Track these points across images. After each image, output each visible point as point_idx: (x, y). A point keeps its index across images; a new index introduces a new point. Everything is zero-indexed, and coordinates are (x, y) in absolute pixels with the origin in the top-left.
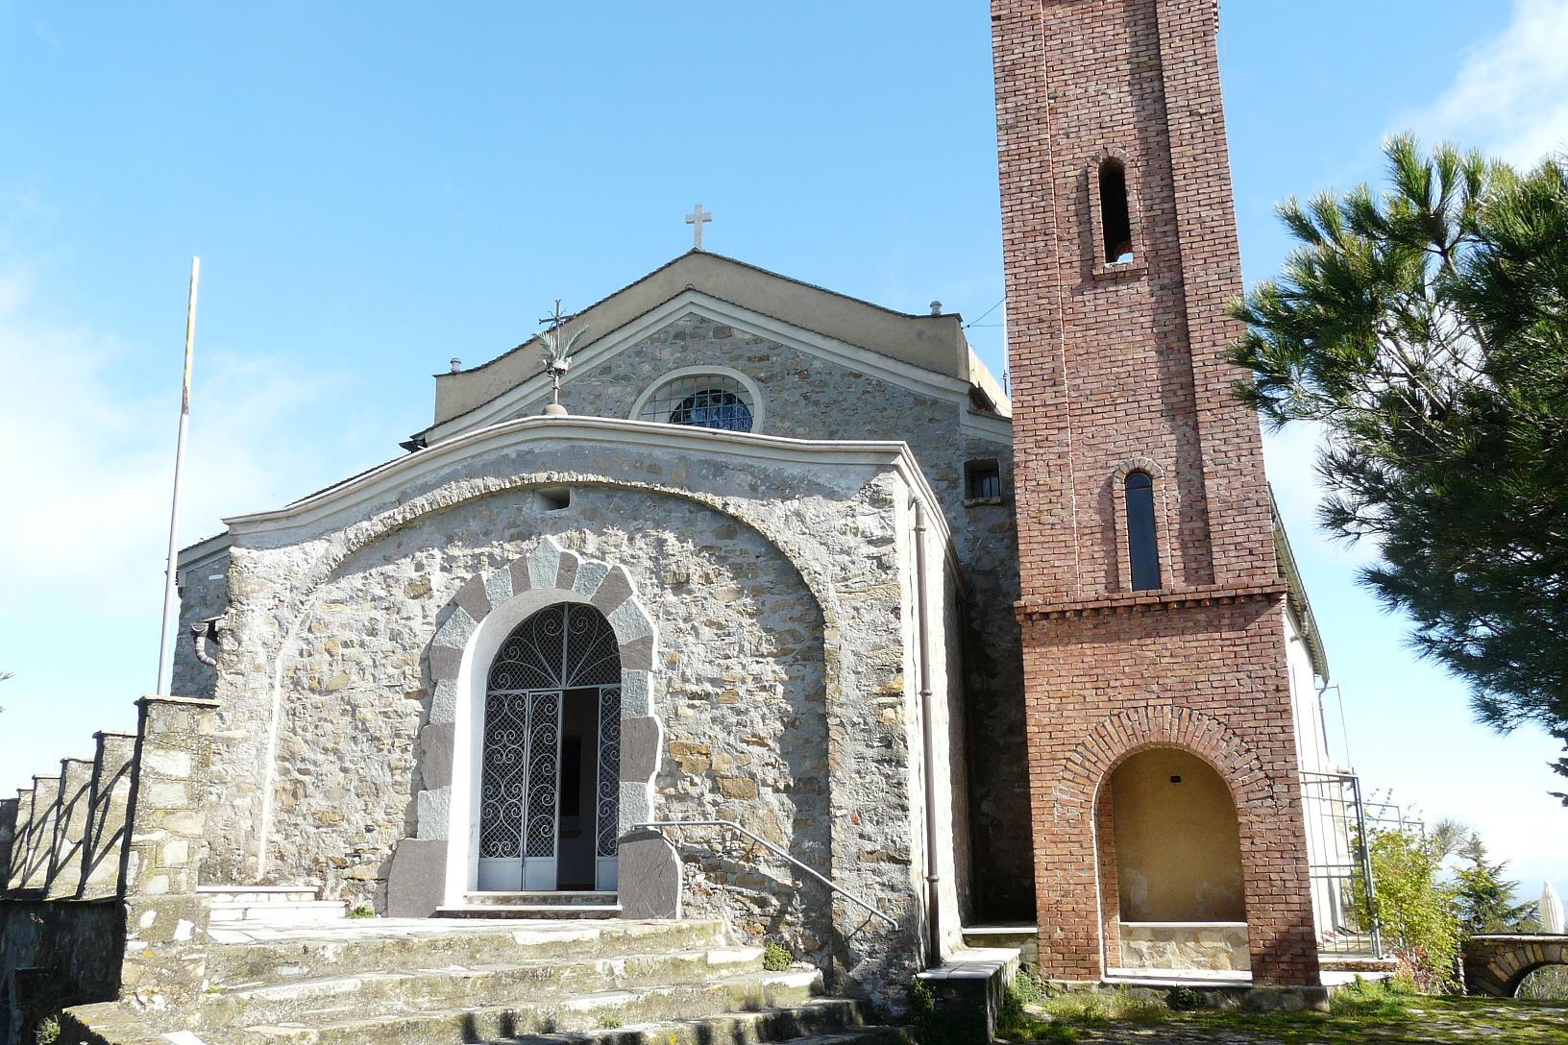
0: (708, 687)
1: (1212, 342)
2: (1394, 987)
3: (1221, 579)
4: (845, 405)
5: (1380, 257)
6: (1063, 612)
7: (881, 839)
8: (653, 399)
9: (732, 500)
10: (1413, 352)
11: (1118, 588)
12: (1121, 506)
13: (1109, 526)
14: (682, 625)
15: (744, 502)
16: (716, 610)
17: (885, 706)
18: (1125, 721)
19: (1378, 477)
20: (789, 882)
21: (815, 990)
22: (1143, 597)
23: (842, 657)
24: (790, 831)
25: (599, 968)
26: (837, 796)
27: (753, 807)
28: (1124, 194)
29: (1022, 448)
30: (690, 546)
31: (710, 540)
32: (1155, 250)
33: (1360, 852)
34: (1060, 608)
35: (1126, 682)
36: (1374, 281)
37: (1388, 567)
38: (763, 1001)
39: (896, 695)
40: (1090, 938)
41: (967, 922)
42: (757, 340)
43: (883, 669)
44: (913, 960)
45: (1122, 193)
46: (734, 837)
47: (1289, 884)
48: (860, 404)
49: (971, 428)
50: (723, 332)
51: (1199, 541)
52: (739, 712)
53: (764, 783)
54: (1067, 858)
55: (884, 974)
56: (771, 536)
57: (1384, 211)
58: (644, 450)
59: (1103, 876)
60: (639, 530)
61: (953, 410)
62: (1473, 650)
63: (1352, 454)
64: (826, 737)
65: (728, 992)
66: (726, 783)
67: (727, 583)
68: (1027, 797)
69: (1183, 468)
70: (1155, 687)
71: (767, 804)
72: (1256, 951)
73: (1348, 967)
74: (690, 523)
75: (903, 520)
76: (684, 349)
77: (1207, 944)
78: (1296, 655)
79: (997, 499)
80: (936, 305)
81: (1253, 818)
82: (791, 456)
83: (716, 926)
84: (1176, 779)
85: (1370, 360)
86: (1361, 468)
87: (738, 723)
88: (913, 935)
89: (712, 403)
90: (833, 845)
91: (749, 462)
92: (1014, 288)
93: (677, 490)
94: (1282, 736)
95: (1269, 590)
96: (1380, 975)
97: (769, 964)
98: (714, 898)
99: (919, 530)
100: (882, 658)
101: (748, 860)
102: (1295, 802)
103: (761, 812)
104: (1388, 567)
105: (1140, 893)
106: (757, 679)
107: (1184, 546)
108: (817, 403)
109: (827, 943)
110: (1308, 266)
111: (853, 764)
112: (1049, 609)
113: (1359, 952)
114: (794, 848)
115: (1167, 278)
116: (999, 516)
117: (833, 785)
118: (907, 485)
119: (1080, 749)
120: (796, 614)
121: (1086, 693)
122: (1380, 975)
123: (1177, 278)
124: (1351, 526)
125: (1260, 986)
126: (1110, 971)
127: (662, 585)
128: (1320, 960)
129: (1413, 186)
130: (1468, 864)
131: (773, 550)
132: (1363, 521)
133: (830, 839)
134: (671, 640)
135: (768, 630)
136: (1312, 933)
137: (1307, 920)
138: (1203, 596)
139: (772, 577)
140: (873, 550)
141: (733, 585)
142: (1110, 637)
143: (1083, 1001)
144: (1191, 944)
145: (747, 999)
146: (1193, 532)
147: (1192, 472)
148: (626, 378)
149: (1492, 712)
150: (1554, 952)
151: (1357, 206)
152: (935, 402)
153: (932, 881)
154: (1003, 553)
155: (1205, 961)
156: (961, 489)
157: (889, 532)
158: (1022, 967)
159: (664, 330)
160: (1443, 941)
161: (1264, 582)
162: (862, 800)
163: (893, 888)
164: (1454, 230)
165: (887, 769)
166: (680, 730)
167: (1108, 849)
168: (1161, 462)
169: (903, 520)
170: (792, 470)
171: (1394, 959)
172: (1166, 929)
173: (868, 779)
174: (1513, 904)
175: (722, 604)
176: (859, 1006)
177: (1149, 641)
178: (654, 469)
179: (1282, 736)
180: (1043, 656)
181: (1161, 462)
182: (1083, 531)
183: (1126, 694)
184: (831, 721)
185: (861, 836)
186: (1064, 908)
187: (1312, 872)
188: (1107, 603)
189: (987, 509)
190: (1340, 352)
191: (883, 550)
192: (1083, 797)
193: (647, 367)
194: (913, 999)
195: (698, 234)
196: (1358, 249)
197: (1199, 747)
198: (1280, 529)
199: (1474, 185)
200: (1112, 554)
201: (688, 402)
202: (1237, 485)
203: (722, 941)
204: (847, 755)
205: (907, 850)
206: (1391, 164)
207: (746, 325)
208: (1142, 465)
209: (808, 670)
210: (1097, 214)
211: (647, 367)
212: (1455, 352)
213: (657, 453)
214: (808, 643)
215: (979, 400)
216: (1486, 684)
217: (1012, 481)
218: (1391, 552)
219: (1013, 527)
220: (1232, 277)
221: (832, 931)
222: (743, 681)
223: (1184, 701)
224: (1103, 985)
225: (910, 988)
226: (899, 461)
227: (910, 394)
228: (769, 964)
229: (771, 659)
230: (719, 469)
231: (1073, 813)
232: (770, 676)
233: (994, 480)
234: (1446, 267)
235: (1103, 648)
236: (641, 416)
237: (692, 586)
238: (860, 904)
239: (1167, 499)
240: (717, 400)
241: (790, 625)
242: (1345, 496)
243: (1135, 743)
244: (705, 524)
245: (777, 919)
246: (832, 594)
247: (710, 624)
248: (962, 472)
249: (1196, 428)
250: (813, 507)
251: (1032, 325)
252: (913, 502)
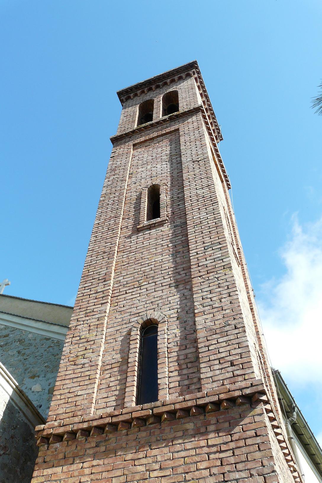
3: (208, 387)
4: (37, 354)
34: (69, 428)
42: (6, 327)
48: (46, 353)
95: (248, 391)
96: (264, 382)
112: (61, 430)
115: (178, 222)
138: (190, 404)
142: (107, 453)
161: (243, 384)
200: (123, 383)
202: (220, 317)
208: (153, 316)
239: (168, 338)
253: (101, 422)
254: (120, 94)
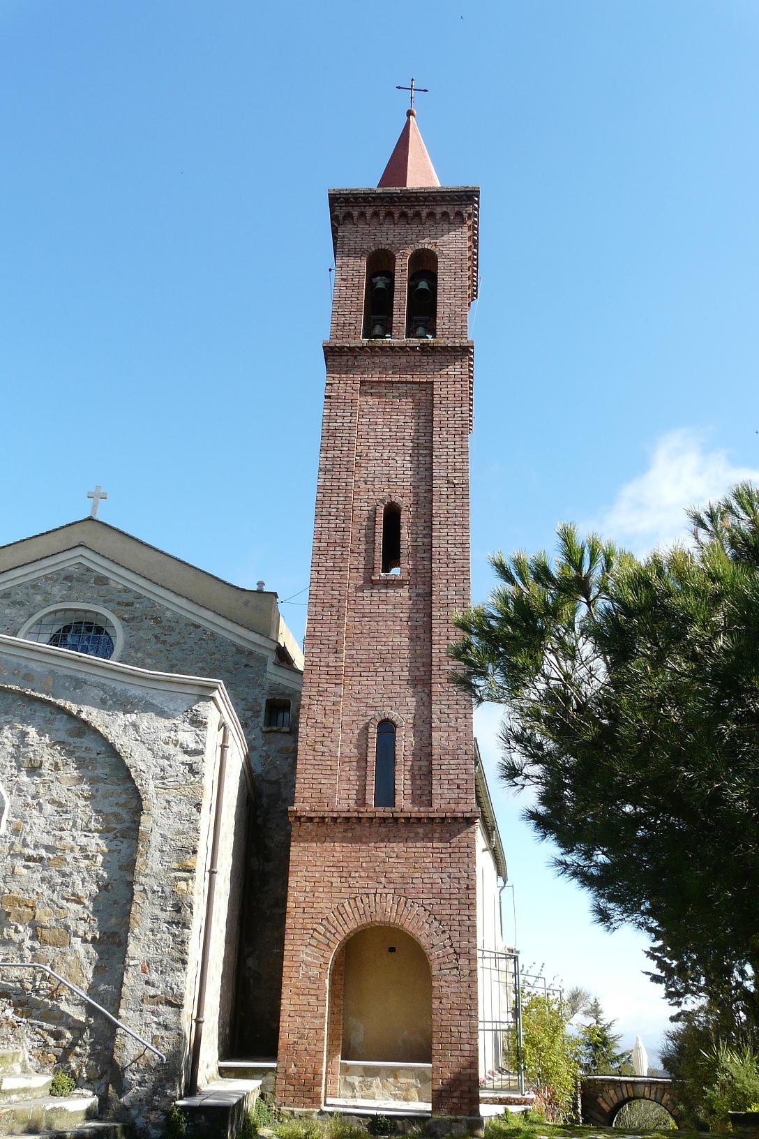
0: (43, 853)
1: (445, 638)
2: (531, 1118)
3: (437, 803)
4: (185, 647)
5: (551, 601)
6: (323, 818)
7: (162, 986)
8: (39, 622)
9: (85, 708)
10: (567, 665)
11: (364, 804)
12: (373, 744)
13: (363, 758)
14: (29, 800)
15: (94, 711)
16: (59, 792)
17: (180, 879)
18: (359, 904)
19: (540, 746)
20: (83, 1019)
21: (90, 1115)
22: (382, 812)
23: (152, 838)
24: (90, 975)
26: (133, 949)
27: (63, 954)
28: (399, 528)
29: (308, 694)
30: (47, 739)
31: (63, 736)
32: (415, 568)
33: (516, 1013)
34: (321, 814)
35: (363, 874)
36: (545, 615)
37: (542, 809)
38: (44, 1124)
39: (190, 871)
40: (316, 1073)
41: (223, 1057)
42: (126, 590)
43: (182, 850)
44: (174, 1089)
45: (398, 527)
46: (44, 978)
47: (464, 1036)
48: (196, 648)
49: (275, 675)
50: (102, 580)
51: (424, 776)
52: (64, 875)
53: (76, 935)
54: (306, 1008)
55: (149, 1101)
56: (111, 739)
57: (555, 571)
58: (24, 663)
59: (331, 1022)
60: (8, 723)
61: (262, 661)
62: (594, 871)
63: (524, 729)
64: (130, 900)
65: (14, 1115)
66: (45, 932)
67: (71, 771)
68: (281, 957)
69: (419, 722)
70: (383, 880)
71: (75, 951)
72: (436, 1087)
73: (501, 1101)
74: (49, 722)
75: (213, 737)
76: (70, 588)
77: (402, 1080)
78: (484, 861)
79: (286, 729)
80: (261, 584)
81: (443, 983)
82: (136, 681)
83: (14, 1056)
84: (392, 950)
85: (538, 669)
86: (529, 740)
87: (62, 884)
88: (178, 1067)
89: (84, 632)
90: (124, 989)
91: (103, 681)
92: (316, 581)
93: (43, 696)
94: (468, 923)
96: (521, 1108)
97: (55, 1090)
98: (18, 1030)
99: (224, 747)
100: (183, 841)
101: (52, 998)
102: (473, 973)
103: (69, 958)
104: (542, 809)
105: (358, 1037)
106: (83, 849)
107: (413, 778)
108: (164, 642)
109: (107, 1073)
110: (505, 599)
111: (148, 923)
112: (313, 815)
113: (510, 1089)
114: (92, 990)
115: (421, 589)
116: (285, 741)
117: (130, 940)
118: (219, 711)
119: (324, 922)
120: (121, 801)
121: (333, 880)
122: (521, 1108)
123: (428, 590)
124: (518, 780)
125: (437, 1116)
126: (329, 1101)
127: (19, 768)
128: (481, 1095)
129: (572, 557)
130: (590, 1021)
131: (112, 751)
132: (527, 777)
133: (122, 984)
134: (19, 811)
135: (97, 812)
136: (477, 1074)
137: (474, 1064)
138: (423, 815)
139: (107, 771)
140: (187, 758)
141: (75, 773)
143: (306, 1126)
144: (391, 1080)
145: (30, 1122)
146: (420, 769)
147: (424, 726)
148: (21, 604)
149: (603, 916)
150: (641, 1090)
151: (538, 565)
152: (251, 653)
153: (198, 1023)
154: (287, 769)
155: (398, 1096)
156: (262, 719)
157: (201, 747)
158: (262, 1096)
159: (58, 573)
160: (566, 1078)
161: (465, 809)
162: (152, 953)
163: (166, 1027)
164: (595, 591)
165: (174, 929)
166: (14, 886)
167: (337, 1001)
168: (404, 716)
169: (213, 737)
170: (134, 692)
171: (532, 1096)
172: (374, 1068)
173: (159, 936)
174: (617, 1052)
175: (65, 787)
176: (124, 1129)
177: (382, 845)
178: (28, 678)
179: (468, 923)
180: (305, 849)
181: (404, 716)
182: (344, 759)
183: (361, 883)
184: (137, 888)
185: (147, 983)
186: (300, 1047)
187: (481, 1026)
188: (355, 814)
189: (279, 736)
190: (520, 660)
191: (195, 759)
192: (322, 960)
193: (39, 598)
194: (170, 1124)
195: (95, 506)
196: (535, 592)
197: (409, 927)
198: (481, 771)
199: (608, 564)
200: (363, 778)
201: (67, 629)
202: (454, 738)
203: (17, 1068)
204: (146, 916)
205: (182, 996)
206: (561, 541)
207: (120, 578)
209: (124, 846)
210: (379, 538)
211: (39, 598)
212: (591, 670)
213: (33, 665)
214: (127, 825)
215: (283, 656)
216: (602, 896)
217: (298, 717)
218: (544, 800)
219: (295, 750)
220: (464, 594)
221: (112, 1062)
222: (72, 850)
223: (402, 893)
224: (322, 1113)
225: (168, 1114)
226: (216, 694)
227: (233, 644)
228: (55, 1090)
229: (96, 834)
230: (79, 684)
231: (314, 972)
232: (94, 848)
233: (287, 715)
234: (590, 614)
235: (349, 847)
236: (28, 634)
237: (43, 771)
238: (137, 1039)
239: (405, 743)
240: (89, 630)
241: (115, 809)
242: (517, 758)
243: (364, 921)
244: (61, 724)
245: (68, 1051)
246: (151, 788)
247: (53, 802)
248: (264, 706)
249: (430, 695)
250: (147, 721)
251: (325, 608)
252: (223, 725)
253: (348, 815)
254: (336, 199)
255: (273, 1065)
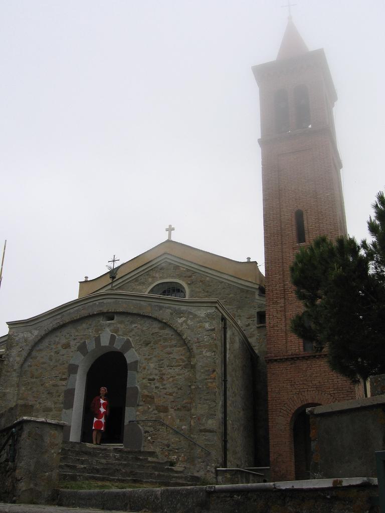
25: (111, 455)
80: (249, 258)
108: (207, 292)
121: (288, 386)
170: (183, 308)
195: (170, 235)
243: (303, 404)
255: (269, 467)
